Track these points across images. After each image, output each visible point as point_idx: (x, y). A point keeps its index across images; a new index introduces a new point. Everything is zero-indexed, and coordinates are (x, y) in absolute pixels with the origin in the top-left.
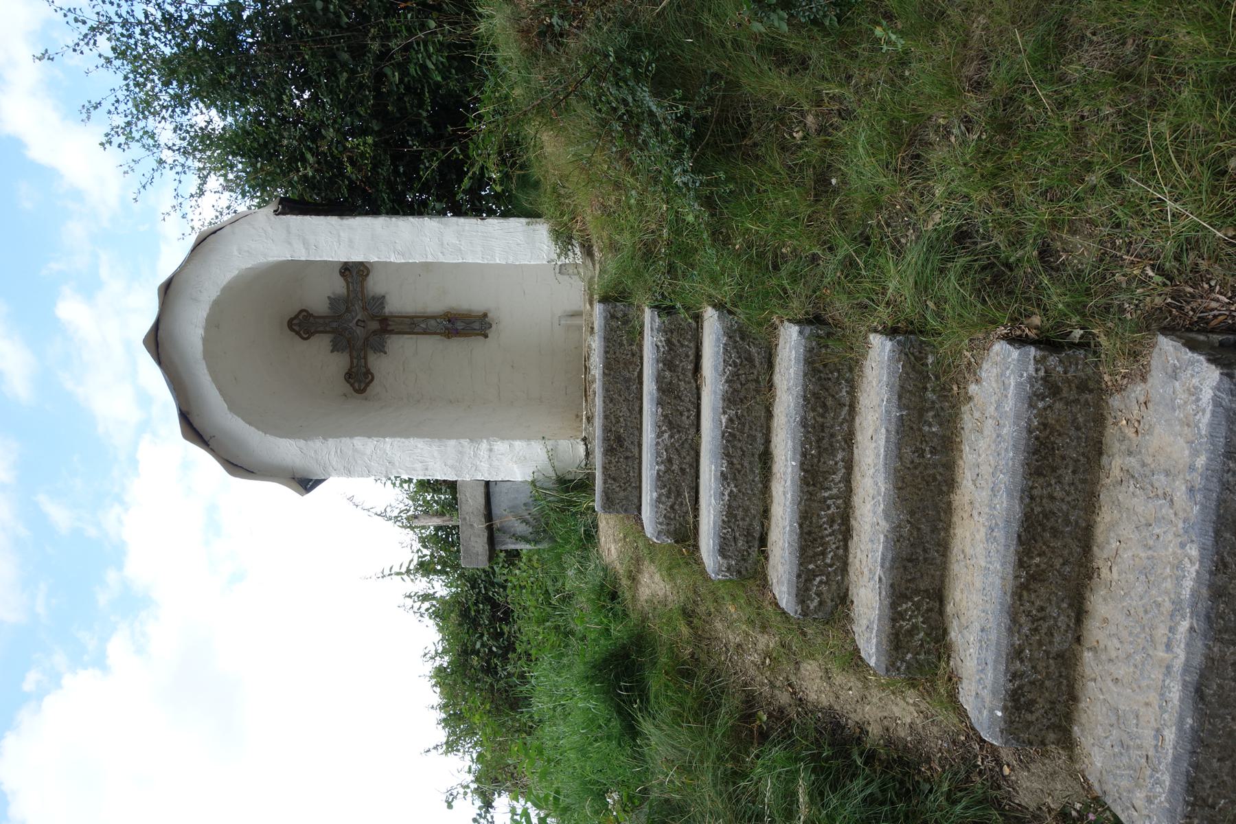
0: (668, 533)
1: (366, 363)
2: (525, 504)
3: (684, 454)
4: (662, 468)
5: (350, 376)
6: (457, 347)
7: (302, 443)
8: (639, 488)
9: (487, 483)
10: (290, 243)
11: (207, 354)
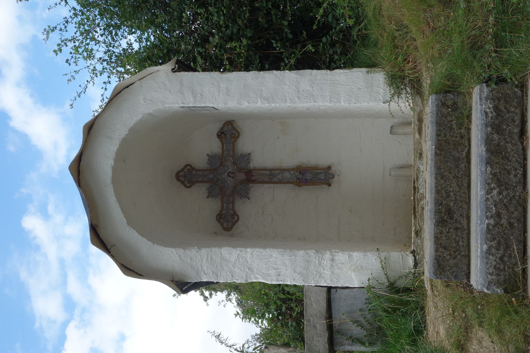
0: (498, 284)
1: (233, 207)
2: (361, 310)
3: (512, 209)
4: (492, 221)
5: (220, 217)
6: (306, 195)
7: (181, 250)
8: (468, 257)
9: (329, 289)
10: (182, 93)
11: (115, 180)
